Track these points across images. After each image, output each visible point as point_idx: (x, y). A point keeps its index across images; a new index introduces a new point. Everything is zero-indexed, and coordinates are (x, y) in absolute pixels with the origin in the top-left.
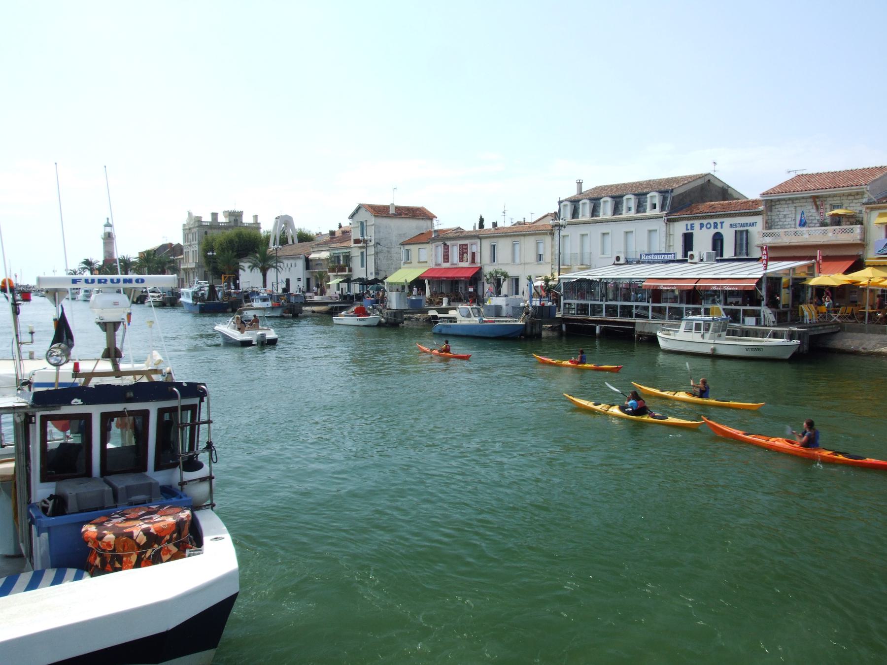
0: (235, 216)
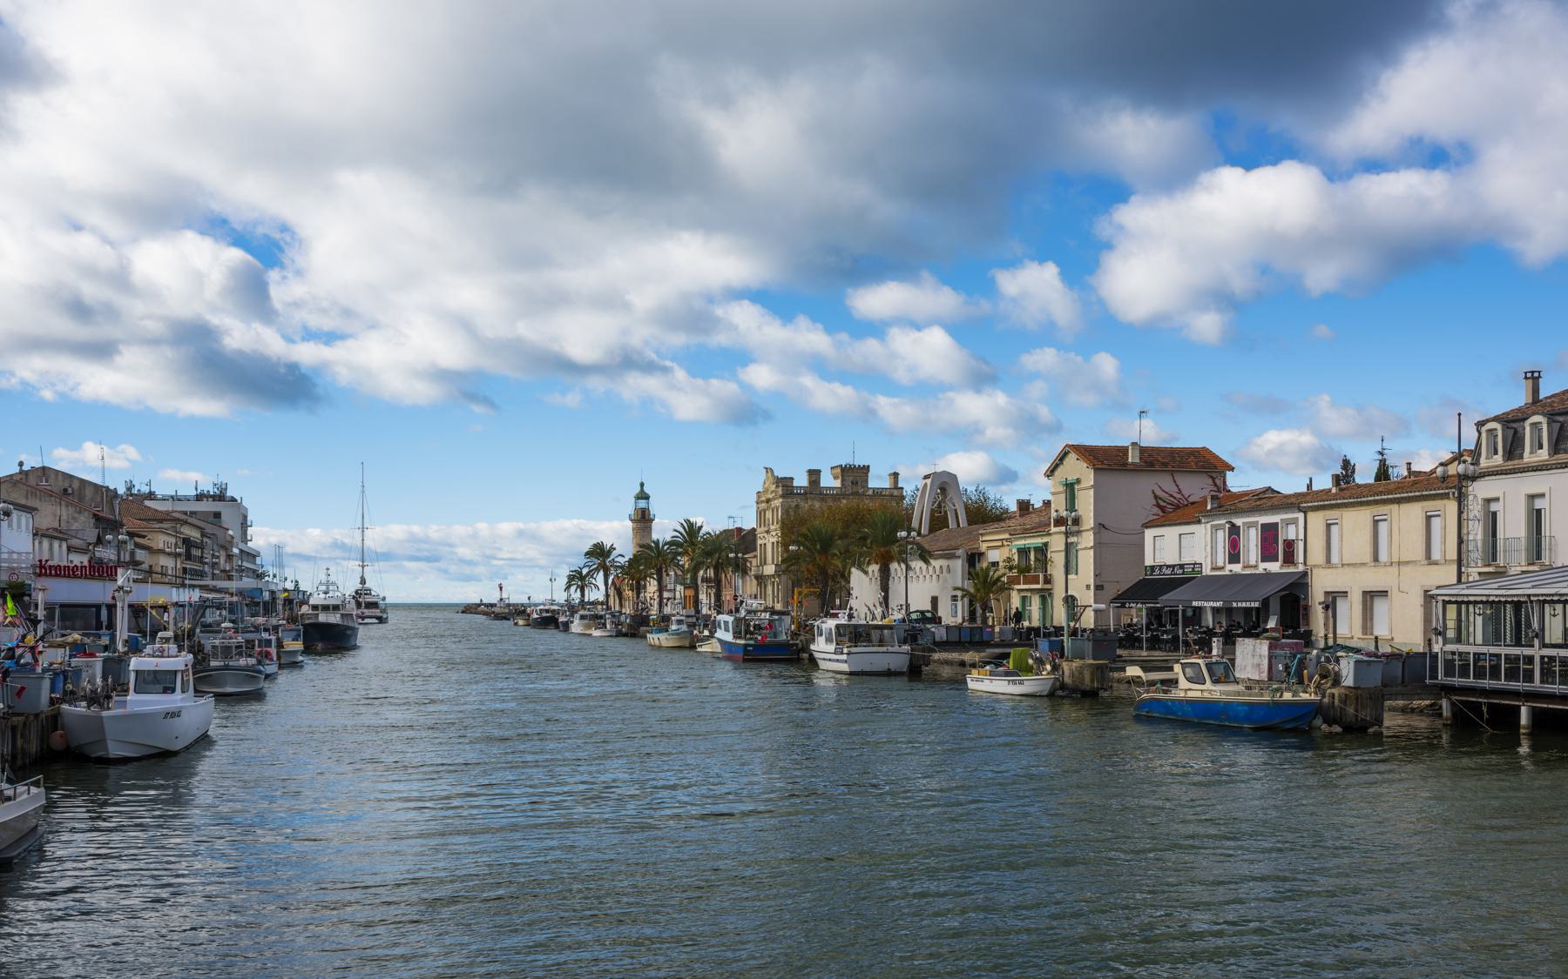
0: (854, 475)
